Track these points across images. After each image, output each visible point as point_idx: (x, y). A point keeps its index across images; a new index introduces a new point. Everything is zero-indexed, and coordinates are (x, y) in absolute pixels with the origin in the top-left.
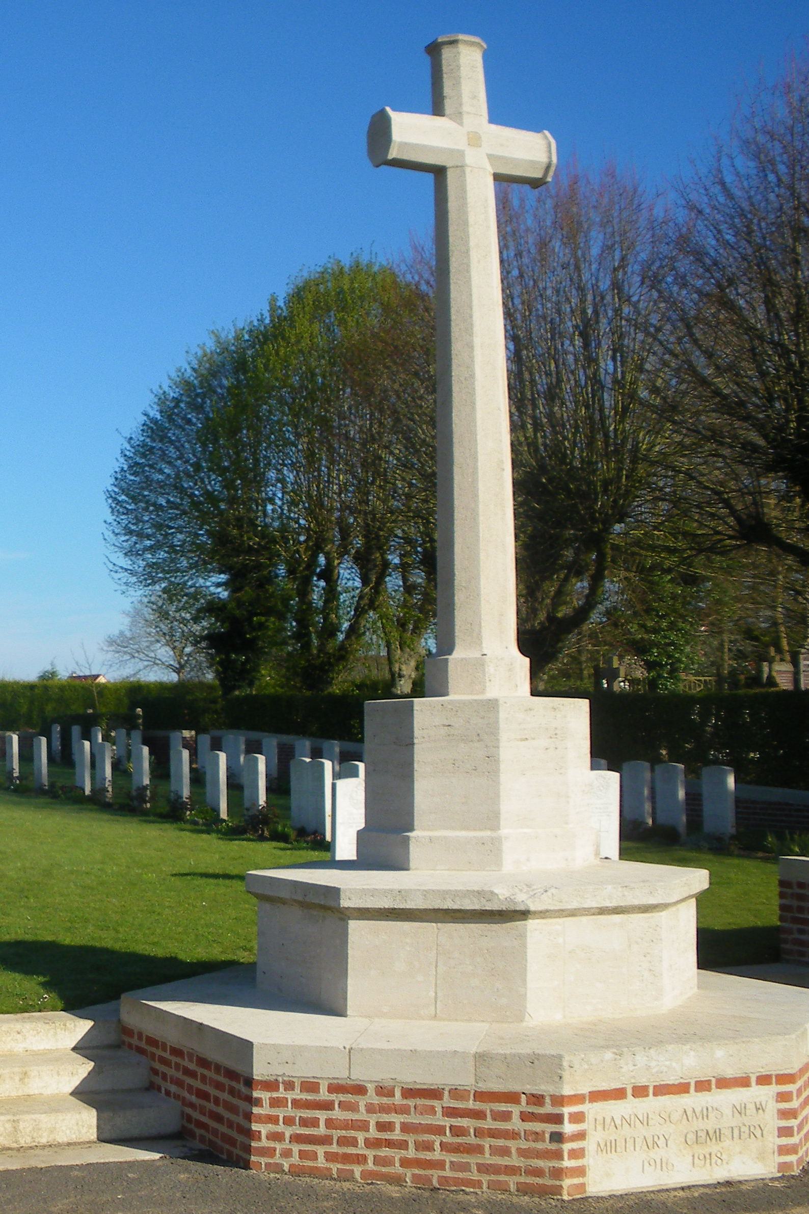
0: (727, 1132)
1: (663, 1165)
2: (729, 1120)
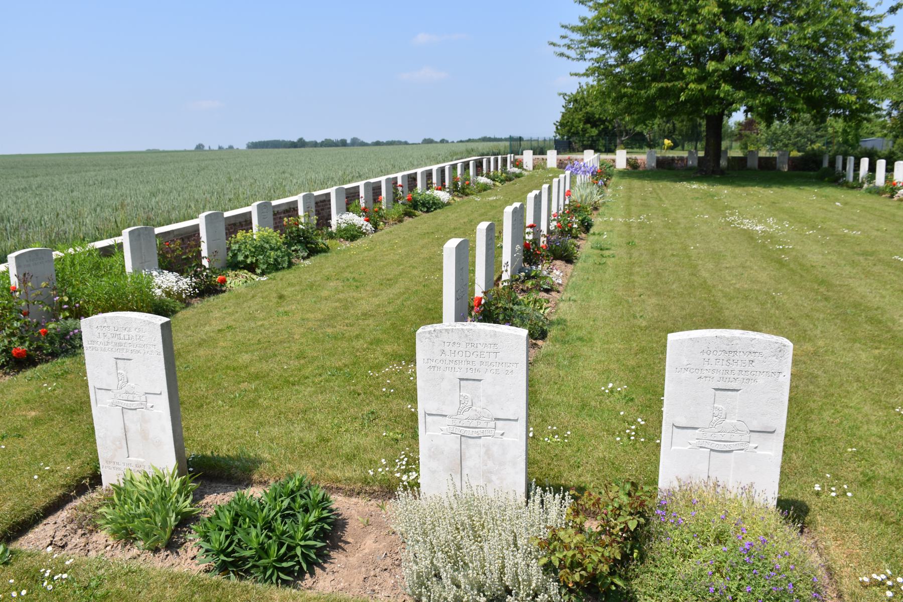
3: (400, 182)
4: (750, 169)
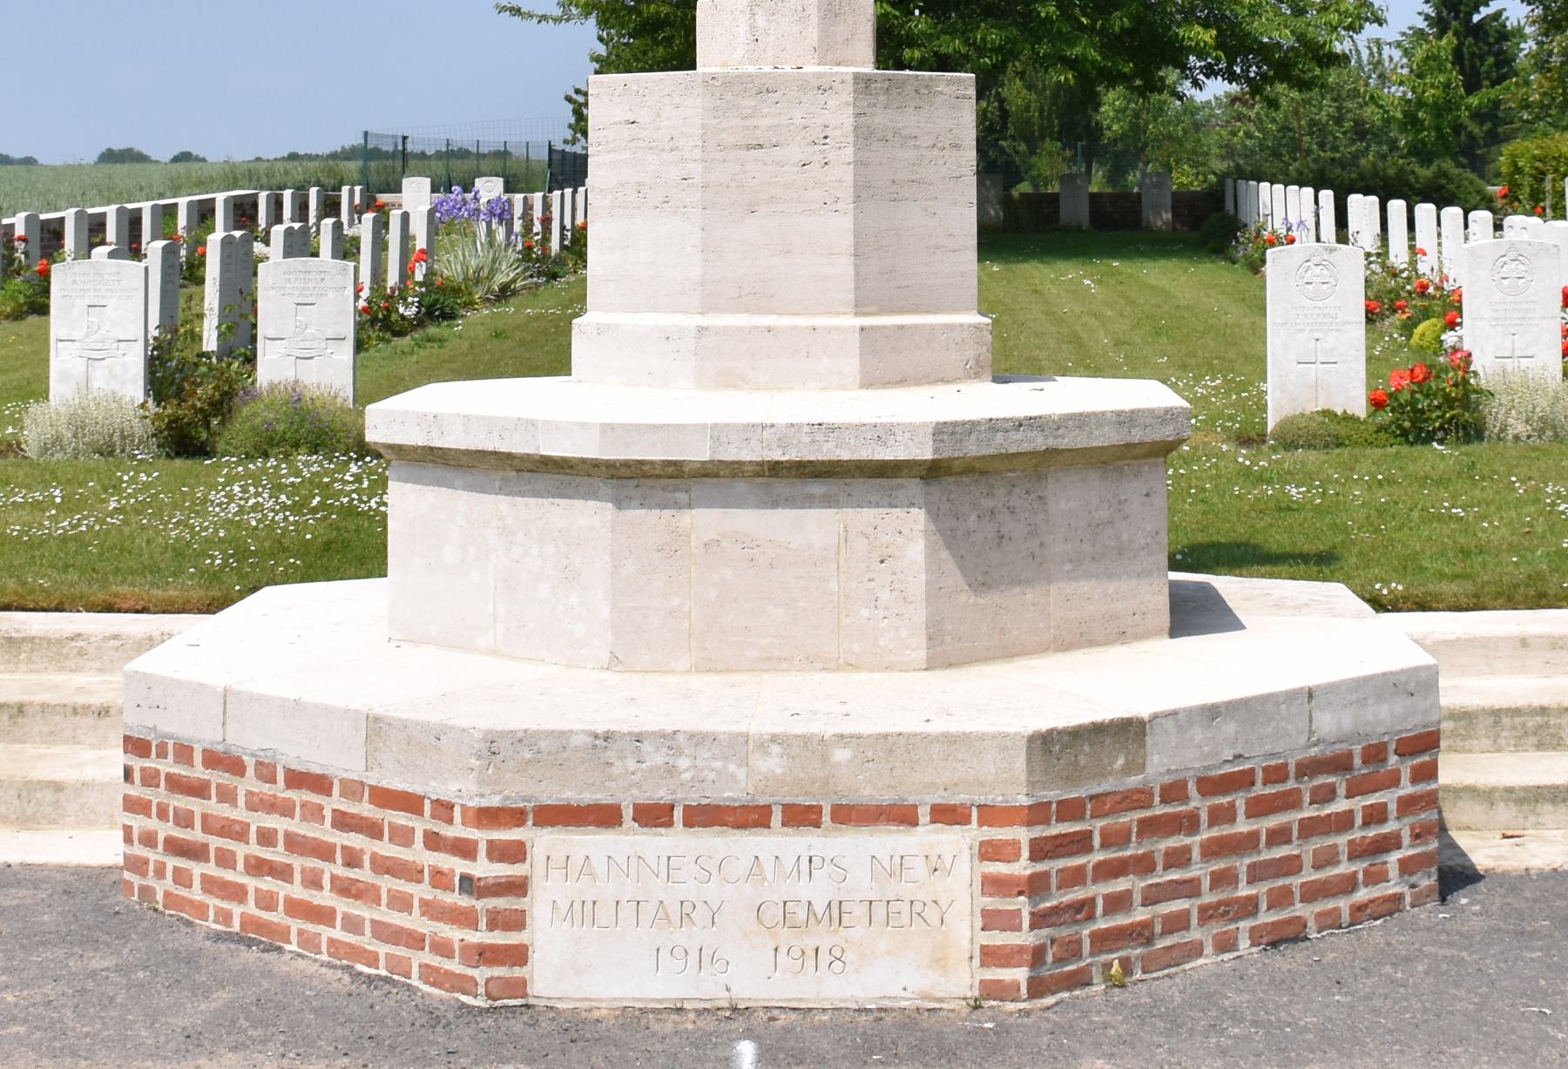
0: (860, 911)
1: (703, 958)
2: (861, 884)
3: (20, 231)
4: (1067, 229)
